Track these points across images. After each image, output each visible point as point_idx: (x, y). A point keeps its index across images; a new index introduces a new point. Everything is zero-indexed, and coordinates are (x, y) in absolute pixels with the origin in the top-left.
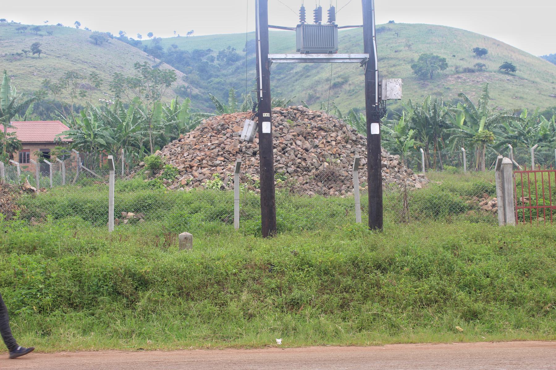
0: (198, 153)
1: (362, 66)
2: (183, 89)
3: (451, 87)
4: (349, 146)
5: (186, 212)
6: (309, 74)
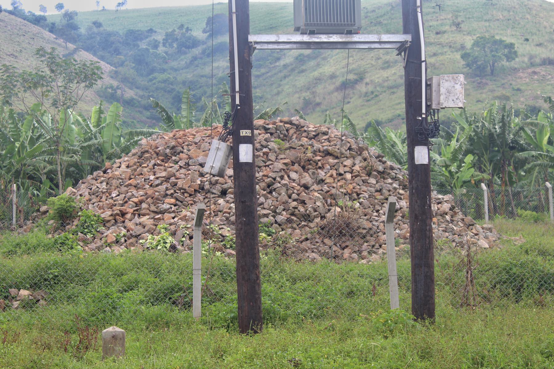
0: (134, 192)
1: (399, 54)
2: (110, 90)
3: (523, 88)
4: (372, 181)
5: (113, 290)
6: (304, 67)
